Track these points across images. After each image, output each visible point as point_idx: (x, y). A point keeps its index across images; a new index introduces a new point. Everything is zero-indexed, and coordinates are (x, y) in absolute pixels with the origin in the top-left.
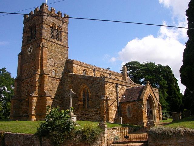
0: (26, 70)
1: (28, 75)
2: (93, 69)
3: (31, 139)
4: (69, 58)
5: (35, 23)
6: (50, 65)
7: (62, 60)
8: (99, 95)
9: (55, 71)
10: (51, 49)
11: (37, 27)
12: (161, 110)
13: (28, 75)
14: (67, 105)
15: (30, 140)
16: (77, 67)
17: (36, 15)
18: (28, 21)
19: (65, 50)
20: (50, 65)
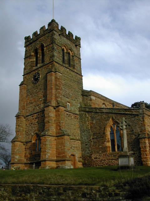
0: (32, 103)
1: (34, 109)
2: (111, 104)
3: (90, 194)
4: (83, 89)
5: (42, 44)
6: (65, 96)
7: (77, 91)
8: (136, 133)
9: (69, 104)
10: (65, 76)
11: (45, 48)
12: (20, 185)
13: (34, 109)
14: (86, 148)
15: (88, 196)
16: (96, 99)
17: (44, 35)
18: (31, 43)
19: (79, 79)
20: (65, 96)
